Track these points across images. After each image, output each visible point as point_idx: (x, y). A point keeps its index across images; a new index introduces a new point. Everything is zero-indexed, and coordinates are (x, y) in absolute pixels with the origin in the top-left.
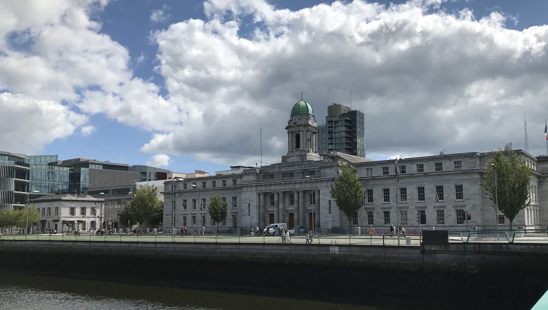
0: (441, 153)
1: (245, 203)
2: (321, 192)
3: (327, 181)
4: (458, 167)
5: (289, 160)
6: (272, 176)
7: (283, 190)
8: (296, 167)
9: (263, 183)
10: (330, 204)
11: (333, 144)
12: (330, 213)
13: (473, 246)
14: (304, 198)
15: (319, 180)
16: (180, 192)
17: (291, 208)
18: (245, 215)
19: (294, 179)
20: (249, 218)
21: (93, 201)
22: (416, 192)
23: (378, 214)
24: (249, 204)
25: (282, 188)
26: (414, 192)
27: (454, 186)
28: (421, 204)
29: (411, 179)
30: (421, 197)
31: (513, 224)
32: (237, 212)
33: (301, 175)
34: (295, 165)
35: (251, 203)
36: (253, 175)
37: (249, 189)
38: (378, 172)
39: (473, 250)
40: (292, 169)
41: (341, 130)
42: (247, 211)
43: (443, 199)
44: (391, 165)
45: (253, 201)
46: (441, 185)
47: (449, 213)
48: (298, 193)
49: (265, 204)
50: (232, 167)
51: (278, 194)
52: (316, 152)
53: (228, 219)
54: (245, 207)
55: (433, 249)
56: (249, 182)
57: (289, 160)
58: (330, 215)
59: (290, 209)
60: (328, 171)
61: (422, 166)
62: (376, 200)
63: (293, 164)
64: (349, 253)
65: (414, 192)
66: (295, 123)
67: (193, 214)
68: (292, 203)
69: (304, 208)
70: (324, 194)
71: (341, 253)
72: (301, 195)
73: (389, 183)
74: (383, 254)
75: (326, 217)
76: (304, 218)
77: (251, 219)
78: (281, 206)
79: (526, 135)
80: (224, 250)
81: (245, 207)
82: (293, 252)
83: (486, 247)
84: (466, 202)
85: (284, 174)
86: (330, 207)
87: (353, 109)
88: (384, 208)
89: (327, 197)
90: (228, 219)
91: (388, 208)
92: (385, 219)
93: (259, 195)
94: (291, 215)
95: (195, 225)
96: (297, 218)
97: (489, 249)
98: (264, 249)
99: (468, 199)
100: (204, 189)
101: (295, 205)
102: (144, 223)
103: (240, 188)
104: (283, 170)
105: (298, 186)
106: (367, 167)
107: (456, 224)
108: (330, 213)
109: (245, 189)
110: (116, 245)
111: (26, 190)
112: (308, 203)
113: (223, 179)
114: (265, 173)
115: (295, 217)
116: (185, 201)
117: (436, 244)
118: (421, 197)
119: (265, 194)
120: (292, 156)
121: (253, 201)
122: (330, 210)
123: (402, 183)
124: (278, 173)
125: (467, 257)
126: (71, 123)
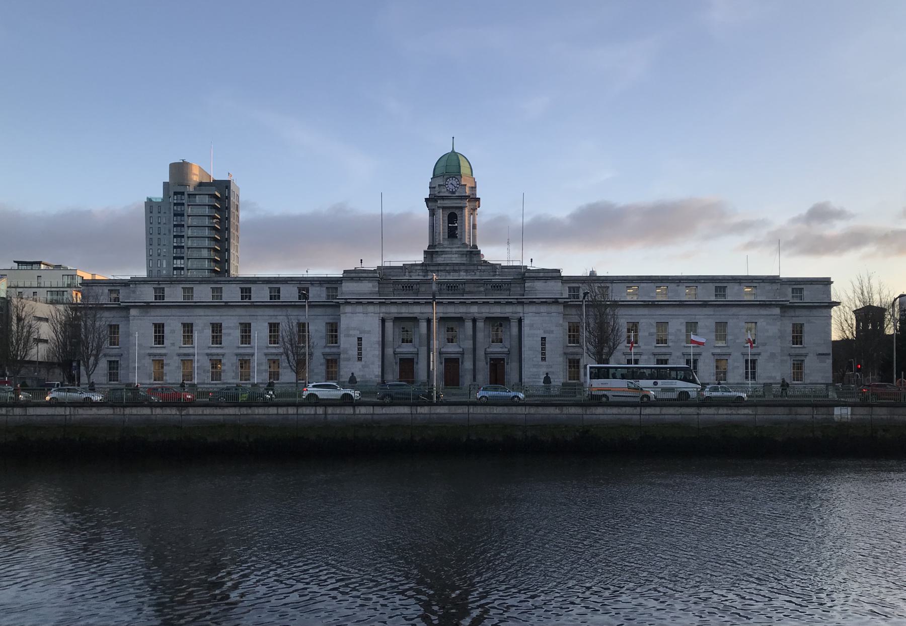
0: (592, 273)
1: (348, 336)
2: (526, 322)
3: (357, 303)
5: (440, 260)
6: (409, 287)
8: (462, 273)
10: (360, 344)
12: (544, 359)
16: (147, 306)
18: (348, 360)
20: (359, 365)
24: (360, 339)
25: (487, 311)
26: (680, 330)
30: (246, 337)
34: (460, 270)
37: (360, 309)
38: (261, 294)
40: (452, 277)
41: (198, 215)
45: (369, 332)
47: (736, 364)
48: (474, 321)
51: (429, 321)
57: (440, 260)
58: (544, 363)
59: (450, 350)
61: (249, 290)
65: (680, 330)
67: (185, 355)
70: (531, 326)
71: (854, 417)
72: (480, 325)
75: (534, 366)
77: (364, 367)
80: (602, 417)
86: (543, 349)
87: (218, 175)
89: (538, 332)
93: (383, 321)
98: (698, 414)
99: (764, 344)
102: (819, 372)
105: (474, 309)
107: (210, 380)
108: (544, 359)
109: (348, 309)
118: (246, 337)
121: (369, 332)
122: (543, 354)
123: (157, 316)
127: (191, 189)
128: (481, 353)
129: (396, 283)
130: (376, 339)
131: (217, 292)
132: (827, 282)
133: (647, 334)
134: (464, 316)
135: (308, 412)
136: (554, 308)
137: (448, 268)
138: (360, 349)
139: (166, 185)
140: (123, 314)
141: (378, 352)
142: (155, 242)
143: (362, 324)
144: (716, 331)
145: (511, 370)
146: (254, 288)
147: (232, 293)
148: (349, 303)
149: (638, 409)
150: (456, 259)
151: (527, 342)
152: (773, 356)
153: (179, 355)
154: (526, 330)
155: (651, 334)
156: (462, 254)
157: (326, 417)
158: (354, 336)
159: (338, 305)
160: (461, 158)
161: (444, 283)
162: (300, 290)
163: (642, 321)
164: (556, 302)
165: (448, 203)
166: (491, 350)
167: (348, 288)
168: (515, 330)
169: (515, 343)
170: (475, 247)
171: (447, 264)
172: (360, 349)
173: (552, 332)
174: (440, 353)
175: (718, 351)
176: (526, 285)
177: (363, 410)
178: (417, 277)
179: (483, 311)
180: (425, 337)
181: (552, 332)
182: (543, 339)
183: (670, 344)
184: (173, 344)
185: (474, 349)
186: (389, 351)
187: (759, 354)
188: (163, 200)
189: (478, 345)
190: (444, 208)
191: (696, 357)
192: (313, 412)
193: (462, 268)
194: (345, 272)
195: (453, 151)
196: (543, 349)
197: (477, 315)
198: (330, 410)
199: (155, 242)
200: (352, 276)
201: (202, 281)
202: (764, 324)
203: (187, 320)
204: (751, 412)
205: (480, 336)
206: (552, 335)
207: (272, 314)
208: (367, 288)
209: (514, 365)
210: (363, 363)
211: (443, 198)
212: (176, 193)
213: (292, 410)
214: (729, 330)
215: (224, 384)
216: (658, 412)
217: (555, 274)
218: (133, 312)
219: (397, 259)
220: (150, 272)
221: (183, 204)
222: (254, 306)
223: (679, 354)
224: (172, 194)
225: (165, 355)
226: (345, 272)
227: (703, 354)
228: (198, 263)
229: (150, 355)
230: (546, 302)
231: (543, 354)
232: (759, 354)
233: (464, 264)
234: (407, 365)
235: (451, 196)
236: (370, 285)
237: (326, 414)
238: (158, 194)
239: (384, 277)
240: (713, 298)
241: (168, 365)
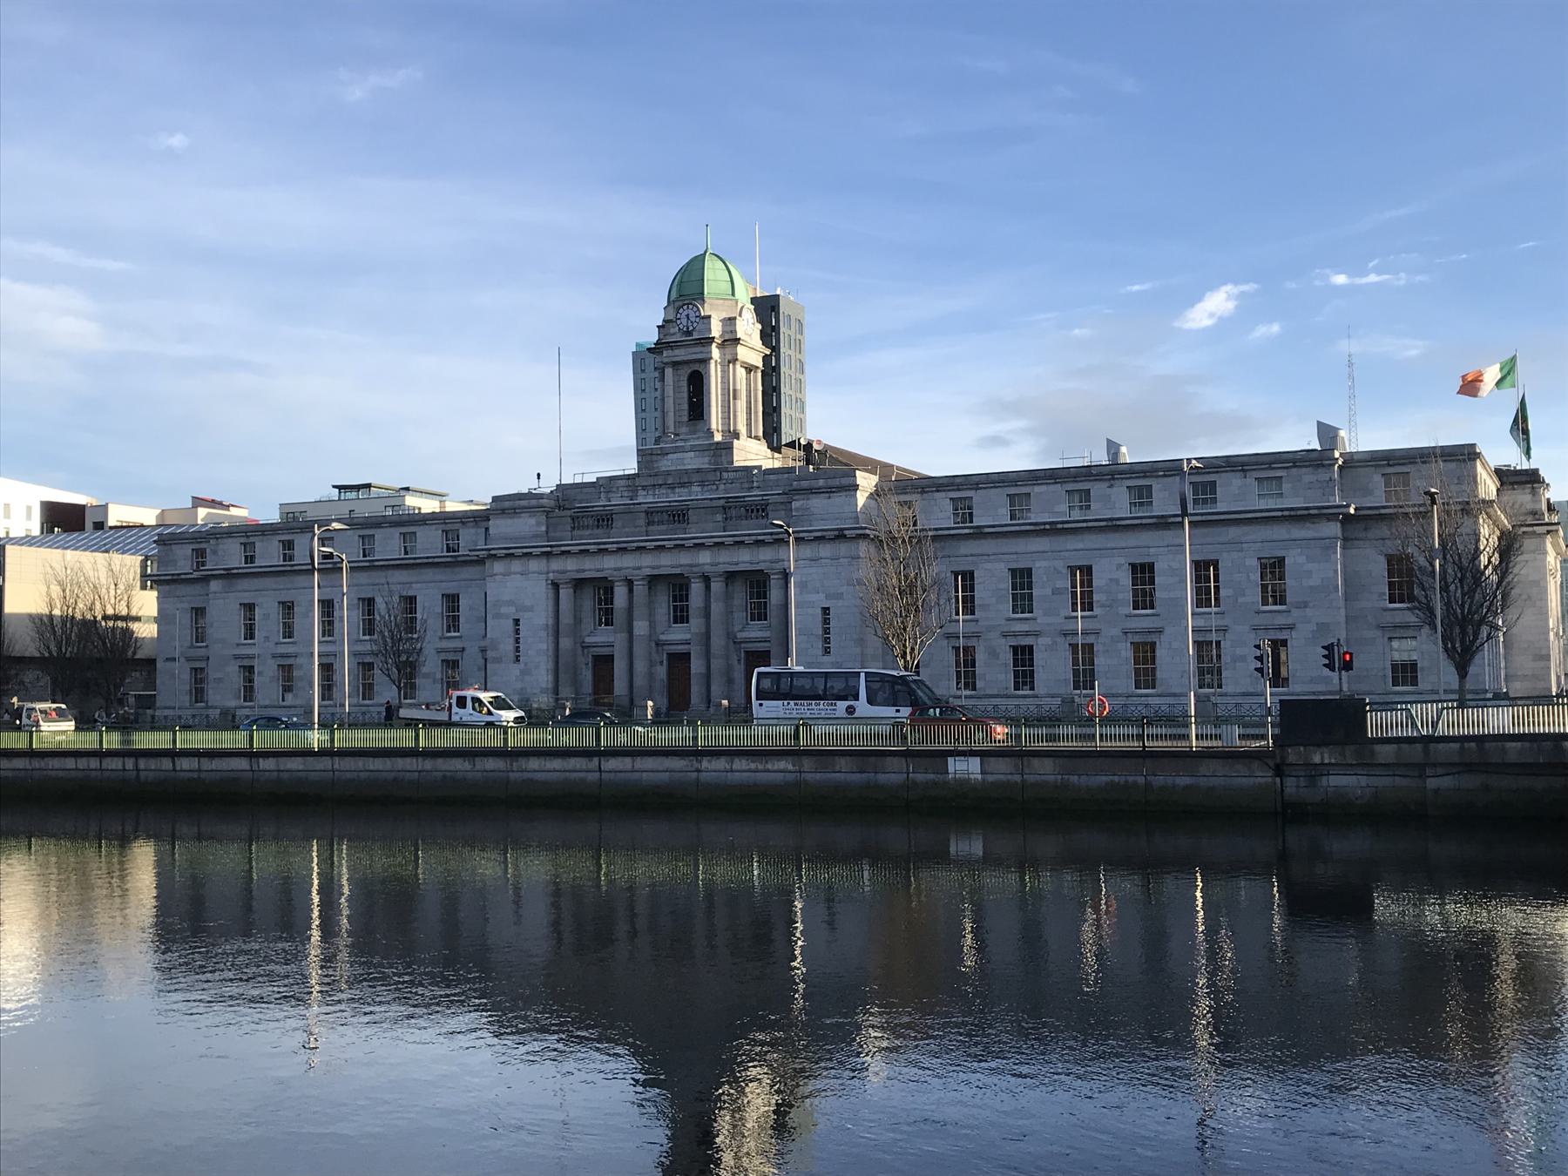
1: (498, 616)
3: (817, 538)
4: (1205, 501)
5: (666, 464)
6: (605, 520)
7: (648, 572)
8: (695, 489)
9: (568, 543)
10: (826, 621)
12: (827, 651)
13: (1456, 746)
14: (728, 597)
15: (768, 538)
16: (229, 575)
17: (677, 634)
18: (498, 660)
19: (694, 533)
20: (515, 670)
22: (1126, 579)
23: (993, 654)
24: (517, 622)
25: (648, 563)
26: (1117, 581)
27: (1255, 563)
28: (1143, 620)
29: (1111, 536)
31: (1468, 686)
32: (464, 649)
33: (719, 517)
35: (525, 618)
36: (532, 514)
37: (516, 566)
39: (1456, 759)
40: (680, 495)
42: (509, 646)
43: (1152, 607)
44: (1037, 489)
45: (530, 609)
46: (1280, 554)
47: (1239, 651)
49: (578, 620)
50: (340, 488)
51: (630, 583)
52: (757, 438)
53: (426, 676)
54: (499, 629)
55: (1317, 759)
56: (517, 539)
57: (666, 464)
58: (826, 658)
60: (817, 503)
62: (985, 607)
63: (683, 479)
64: (1017, 778)
65: (1117, 581)
66: (689, 333)
67: (282, 656)
68: (681, 616)
69: (731, 636)
71: (990, 778)
72: (717, 586)
73: (1069, 547)
74: (1141, 780)
76: (729, 670)
77: (525, 672)
78: (641, 627)
79: (1352, 397)
80: (538, 776)
81: (499, 629)
82: (809, 777)
83: (1504, 750)
84: (1295, 612)
85: (652, 515)
86: (826, 631)
88: (1015, 635)
89: (813, 597)
90: (426, 676)
91: (1027, 634)
92: (1016, 675)
93: (556, 586)
94: (679, 661)
95: (289, 696)
96: (703, 670)
97: (1512, 758)
98: (698, 771)
99: (1305, 605)
100: (250, 573)
101: (696, 623)
103: (480, 562)
104: (644, 498)
105: (704, 558)
106: (1013, 491)
108: (827, 651)
109: (498, 567)
110: (82, 763)
112: (740, 616)
113: (404, 530)
115: (696, 666)
116: (250, 608)
117: (1326, 744)
119: (579, 584)
120: (676, 450)
121: (530, 609)
122: (827, 640)
123: (246, 591)
124: (628, 511)
125: (1432, 783)
130: (542, 621)
134: (685, 571)
138: (517, 641)
143: (521, 593)
146: (977, 497)
148: (625, 549)
149: (596, 760)
150: (692, 461)
153: (274, 656)
157: (138, 776)
158: (507, 616)
159: (206, 579)
165: (681, 354)
172: (517, 641)
179: (587, 567)
181: (839, 596)
182: (826, 610)
187: (1291, 628)
190: (676, 365)
191: (1090, 639)
193: (695, 478)
196: (826, 631)
197: (707, 568)
200: (506, 506)
202: (1302, 559)
203: (286, 596)
204: (790, 767)
206: (840, 603)
207: (404, 579)
208: (527, 526)
210: (522, 666)
216: (629, 767)
218: (215, 585)
222: (979, 534)
223: (1116, 632)
226: (495, 499)
227: (1168, 630)
229: (236, 657)
230: (822, 538)
232: (1291, 628)
236: (533, 521)
237: (138, 770)
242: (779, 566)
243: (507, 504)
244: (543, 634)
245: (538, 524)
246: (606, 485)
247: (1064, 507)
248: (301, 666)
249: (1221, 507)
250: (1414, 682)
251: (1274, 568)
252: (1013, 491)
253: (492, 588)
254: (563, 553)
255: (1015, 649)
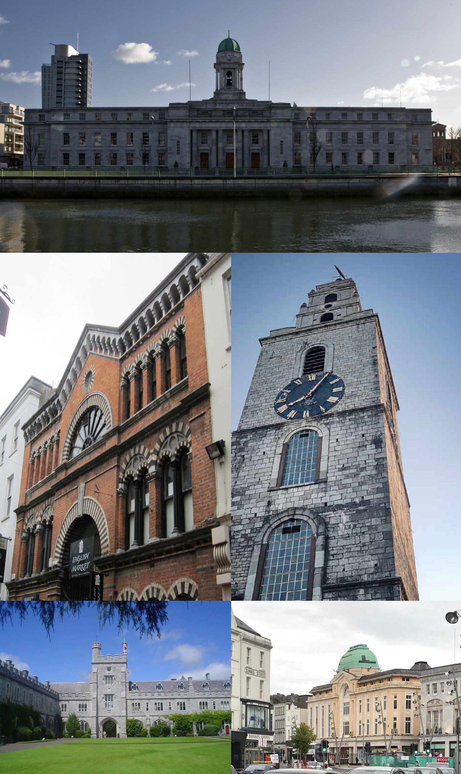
2: (272, 132)
6: (205, 113)
7: (224, 128)
10: (281, 145)
11: (61, 103)
12: (282, 153)
15: (266, 120)
18: (172, 153)
20: (178, 156)
21: (46, 591)
24: (178, 142)
25: (224, 126)
34: (234, 103)
35: (181, 141)
36: (184, 110)
37: (179, 125)
41: (71, 72)
48: (243, 132)
51: (217, 132)
53: (136, 158)
67: (81, 150)
70: (275, 135)
72: (246, 134)
84: (397, 146)
86: (282, 147)
89: (277, 138)
90: (136, 158)
93: (192, 132)
109: (172, 125)
111: (232, 148)
114: (193, 109)
121: (184, 138)
122: (282, 150)
126: (330, 685)
127: (67, 59)
128: (246, 150)
129: (198, 110)
131: (83, 116)
132: (429, 111)
133: (337, 139)
135: (165, 183)
136: (287, 124)
137: (227, 102)
138: (178, 148)
139: (53, 57)
140: (47, 128)
141: (188, 149)
142: (47, 88)
144: (373, 137)
145: (263, 158)
147: (90, 117)
148: (173, 122)
149: (348, 180)
150: (231, 97)
151: (272, 143)
152: (403, 150)
154: (272, 137)
155: (339, 139)
156: (234, 94)
157: (175, 186)
159: (166, 123)
160: (234, 41)
161: (226, 110)
162: (144, 114)
163: (334, 132)
164: (288, 121)
165: (226, 66)
166: (252, 148)
167: (173, 114)
168: (266, 137)
169: (266, 144)
170: (242, 90)
171: (227, 100)
172: (178, 148)
173: (286, 138)
174: (224, 150)
175: (374, 148)
176: (272, 111)
177: (196, 182)
178: (210, 107)
180: (219, 140)
182: (282, 142)
183: (349, 144)
184: (74, 145)
185: (243, 148)
186: (195, 149)
188: (8, 59)
189: (245, 145)
192: (168, 183)
193: (235, 102)
194: (170, 104)
195: (229, 38)
196: (282, 147)
198: (178, 182)
199: (47, 88)
200: (173, 106)
201: (74, 110)
205: (246, 140)
208: (183, 113)
209: (266, 157)
210: (180, 155)
211: (224, 63)
212: (58, 61)
213: (156, 182)
214: (380, 137)
215: (102, 167)
217: (287, 106)
219: (198, 97)
220: (43, 105)
221: (62, 67)
222: (119, 123)
224: (56, 62)
225: (70, 151)
226: (170, 104)
228: (70, 101)
231: (282, 150)
233: (236, 100)
234: (204, 157)
235: (66, 77)
236: (184, 111)
237: (175, 184)
238: (48, 62)
239: (191, 106)
240: (371, 119)
241: (72, 156)
242: (267, 129)
243: (175, 106)
244: (188, 146)
245: (186, 112)
246: (205, 102)
247: (340, 117)
248: (88, 154)
249: (71, 120)
250: (132, 164)
251: (391, 135)
252: (112, 112)
253: (170, 132)
254: (197, 122)
255: (64, 154)
